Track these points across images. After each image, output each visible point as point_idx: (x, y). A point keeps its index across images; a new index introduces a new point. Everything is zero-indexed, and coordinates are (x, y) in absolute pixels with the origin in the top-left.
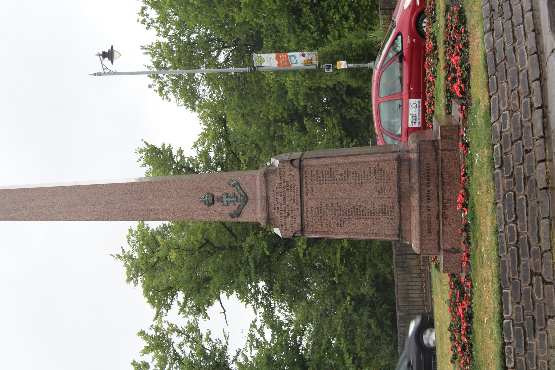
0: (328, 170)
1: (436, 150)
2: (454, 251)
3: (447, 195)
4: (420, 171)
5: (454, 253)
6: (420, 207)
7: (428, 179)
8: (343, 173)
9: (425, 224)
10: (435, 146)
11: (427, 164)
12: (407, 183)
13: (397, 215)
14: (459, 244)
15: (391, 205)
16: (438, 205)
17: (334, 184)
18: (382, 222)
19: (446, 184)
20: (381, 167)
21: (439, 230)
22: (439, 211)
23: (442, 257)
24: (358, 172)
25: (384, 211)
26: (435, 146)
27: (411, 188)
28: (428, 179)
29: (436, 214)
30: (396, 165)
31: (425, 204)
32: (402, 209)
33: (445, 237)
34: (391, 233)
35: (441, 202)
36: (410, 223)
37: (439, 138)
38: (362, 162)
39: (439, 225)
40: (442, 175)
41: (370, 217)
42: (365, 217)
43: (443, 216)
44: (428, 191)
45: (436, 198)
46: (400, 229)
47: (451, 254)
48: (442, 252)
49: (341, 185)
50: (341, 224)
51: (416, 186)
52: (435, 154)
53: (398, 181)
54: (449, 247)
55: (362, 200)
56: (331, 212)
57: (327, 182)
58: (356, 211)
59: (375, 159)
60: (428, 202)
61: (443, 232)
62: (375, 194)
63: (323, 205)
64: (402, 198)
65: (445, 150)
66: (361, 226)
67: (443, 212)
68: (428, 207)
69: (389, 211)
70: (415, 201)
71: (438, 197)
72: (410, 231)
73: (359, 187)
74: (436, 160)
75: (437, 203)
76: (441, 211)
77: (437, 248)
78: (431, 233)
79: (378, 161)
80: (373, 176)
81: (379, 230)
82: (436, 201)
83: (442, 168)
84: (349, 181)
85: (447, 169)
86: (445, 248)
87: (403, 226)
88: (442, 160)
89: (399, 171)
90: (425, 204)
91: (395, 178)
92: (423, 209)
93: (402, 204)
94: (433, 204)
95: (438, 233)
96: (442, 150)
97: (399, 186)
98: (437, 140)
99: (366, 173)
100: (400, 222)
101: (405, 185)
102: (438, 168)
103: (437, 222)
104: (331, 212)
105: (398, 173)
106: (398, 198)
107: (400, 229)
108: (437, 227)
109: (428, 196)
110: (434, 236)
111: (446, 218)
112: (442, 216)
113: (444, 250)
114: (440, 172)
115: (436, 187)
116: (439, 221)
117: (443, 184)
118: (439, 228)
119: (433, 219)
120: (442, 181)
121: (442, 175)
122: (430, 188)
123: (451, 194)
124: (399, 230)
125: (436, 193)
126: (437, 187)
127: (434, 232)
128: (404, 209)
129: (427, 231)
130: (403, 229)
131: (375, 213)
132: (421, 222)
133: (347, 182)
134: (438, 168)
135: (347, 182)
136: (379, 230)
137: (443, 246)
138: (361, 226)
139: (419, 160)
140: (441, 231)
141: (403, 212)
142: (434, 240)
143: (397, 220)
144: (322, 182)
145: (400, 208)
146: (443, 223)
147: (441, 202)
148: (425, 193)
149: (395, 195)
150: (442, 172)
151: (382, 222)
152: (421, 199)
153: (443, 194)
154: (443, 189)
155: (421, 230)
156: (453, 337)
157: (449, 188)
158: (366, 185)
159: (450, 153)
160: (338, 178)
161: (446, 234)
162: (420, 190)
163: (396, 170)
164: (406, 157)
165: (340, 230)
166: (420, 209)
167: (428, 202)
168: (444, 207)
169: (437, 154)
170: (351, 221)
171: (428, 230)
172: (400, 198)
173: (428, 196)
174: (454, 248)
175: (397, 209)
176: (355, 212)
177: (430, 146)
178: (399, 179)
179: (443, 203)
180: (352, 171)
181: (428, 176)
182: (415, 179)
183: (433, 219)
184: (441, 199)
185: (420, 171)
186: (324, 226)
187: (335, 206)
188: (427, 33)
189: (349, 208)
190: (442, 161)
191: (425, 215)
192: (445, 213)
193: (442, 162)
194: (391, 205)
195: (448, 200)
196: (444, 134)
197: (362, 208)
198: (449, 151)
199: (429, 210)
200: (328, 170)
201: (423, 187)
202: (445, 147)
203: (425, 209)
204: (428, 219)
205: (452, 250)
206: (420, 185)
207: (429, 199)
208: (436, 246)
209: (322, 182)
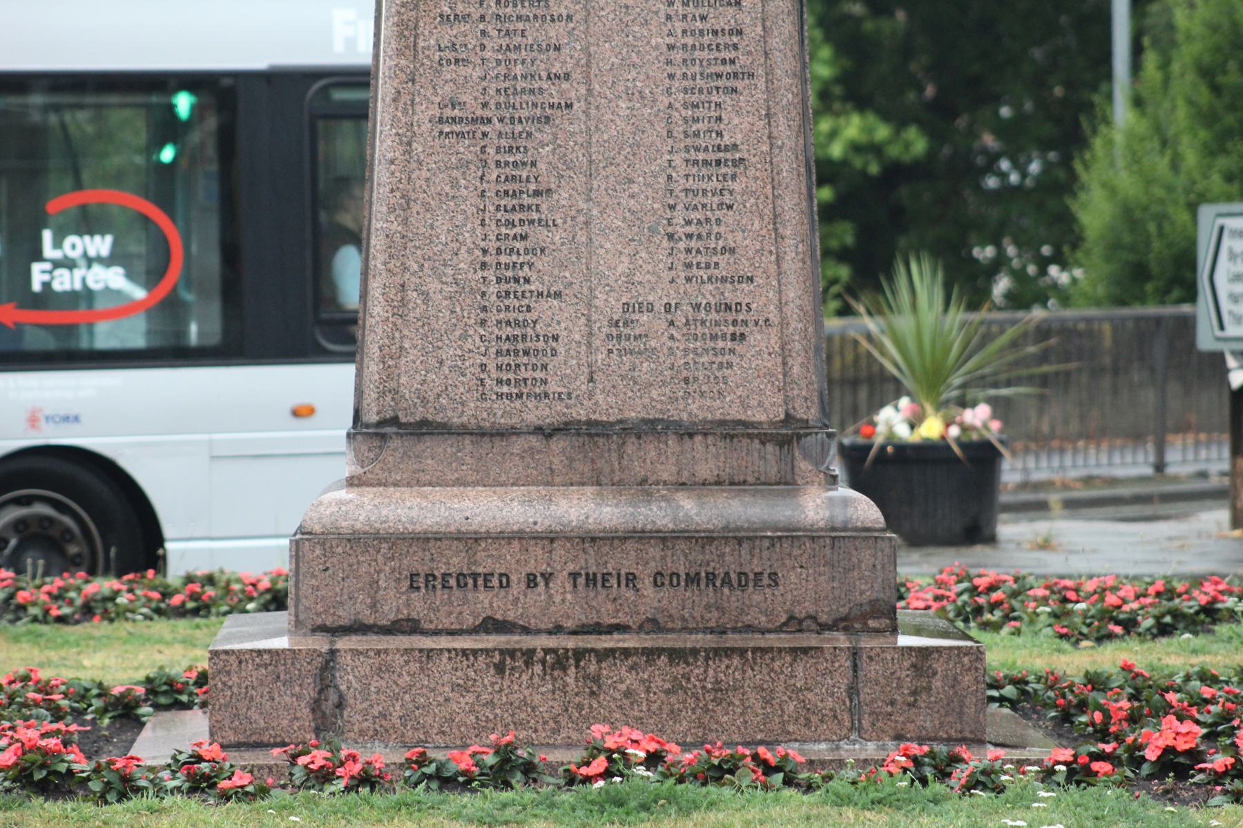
0: (743, 60)
1: (842, 623)
2: (328, 707)
3: (620, 677)
4: (738, 537)
5: (316, 706)
6: (550, 538)
7: (693, 579)
8: (727, 140)
9: (456, 562)
10: (864, 617)
11: (773, 576)
12: (666, 472)
13: (501, 413)
14: (362, 733)
15: (553, 387)
16: (557, 630)
17: (668, 92)
18: (464, 337)
19: (680, 669)
20: (756, 338)
21: (424, 633)
22: (526, 630)
23: (282, 643)
24: (730, 217)
25: (520, 348)
26: (864, 617)
27: (644, 487)
28: (693, 579)
29: (511, 616)
30: (761, 417)
31: (563, 561)
32: (535, 441)
33: (399, 660)
34: (408, 384)
35: (571, 643)
36: (461, 483)
37: (904, 640)
38: (779, 238)
39: (451, 633)
40: (729, 652)
41: (491, 275)
42: (492, 245)
43: (512, 653)
44: (631, 579)
45: (593, 618)
46: (424, 429)
47: (310, 692)
48: (321, 644)
49: (661, 128)
50: (455, 123)
51: (655, 514)
52: (824, 618)
53: (679, 423)
54: (348, 679)
55: (582, 238)
56: (518, 70)
57: (678, 56)
58: (526, 200)
59: (792, 310)
60: (574, 576)
61: (429, 653)
62: (609, 304)
63: (555, 32)
64: (592, 444)
65: (855, 667)
66: (442, 225)
67: (531, 652)
68: (547, 577)
69: (523, 374)
70: (580, 508)
71: (598, 629)
72: (415, 482)
73: (649, 220)
74: (794, 623)
75: (569, 624)
76: (528, 642)
77: (329, 622)
78: (413, 588)
79: (784, 324)
80: (708, 294)
81: (424, 320)
82: (579, 616)
83: (764, 651)
84: (683, 169)
85: (756, 676)
86: (345, 660)
87: (444, 447)
88: (805, 651)
89: (732, 431)
90: (563, 561)
91: (695, 409)
92: (537, 551)
93: (559, 444)
94: (565, 602)
95: (411, 627)
96: (855, 654)
97: (650, 429)
98: (894, 630)
99: (722, 260)
100: (463, 432)
101: (660, 459)
102: (749, 628)
103: (469, 621)
104: (518, 70)
105: (722, 423)
106: (589, 423)
107: (424, 429)
108: (446, 623)
109: (605, 577)
110: (393, 606)
111: (500, 669)
112: (509, 650)
113: (333, 652)
114: (733, 640)
115: (653, 621)
116: (474, 631)
117: (676, 655)
118: (437, 633)
119: (486, 602)
120: (695, 652)
121: (729, 652)
122: (648, 590)
123: (628, 694)
124: (424, 423)
125: (621, 619)
126: (653, 625)
127: (418, 606)
128: (532, 451)
129: (423, 570)
130: (428, 442)
131: (512, 302)
132: (471, 540)
133: (678, 160)
134: (749, 628)
135: (678, 160)
136: (424, 320)
137: (356, 653)
138: (442, 225)
139: (792, 536)
140: (428, 643)
141: (518, 444)
142: (373, 606)
143: (471, 412)
144: (679, 26)
145: (538, 430)
146: (475, 652)
147: (571, 643)
148: (622, 560)
149: (605, 405)
150: (742, 652)
151: (464, 337)
152: (590, 539)
153: (626, 653)
154: (651, 654)
155: (425, 539)
156: (842, 625)
157: (660, 684)
158: (662, 255)
159: (841, 691)
160: (700, 113)
161: (414, 667)
162: (640, 536)
163: (735, 413)
164: (803, 465)
165: (425, 113)
166: (536, 537)
167: (574, 576)
168: (560, 661)
169: (823, 627)
170: (474, 172)
171: (430, 576)
172: (592, 432)
173: (605, 577)
174: (340, 705)
175: (535, 413)
176: (519, 201)
177: (866, 591)
178: (686, 432)
179: (579, 654)
180: (737, 186)
181: (711, 577)
182: (691, 510)
183: (486, 602)
184: (606, 642)
185: (739, 541)
186: (448, 34)
187: (553, 93)
188: (1099, 606)
189: (542, 166)
190: (796, 652)
191: (508, 560)
192: (528, 664)
193: (793, 651)
194: (553, 387)
195: (596, 679)
196: (939, 667)
197: (540, 235)
198: (853, 691)
199: (531, 581)
200: (743, 60)
201: (654, 551)
202: (871, 670)
203: (537, 560)
204: (487, 577)
205: (333, 697)
206: (665, 538)
207: (591, 580)
208: (345, 616)
209: (679, 26)
